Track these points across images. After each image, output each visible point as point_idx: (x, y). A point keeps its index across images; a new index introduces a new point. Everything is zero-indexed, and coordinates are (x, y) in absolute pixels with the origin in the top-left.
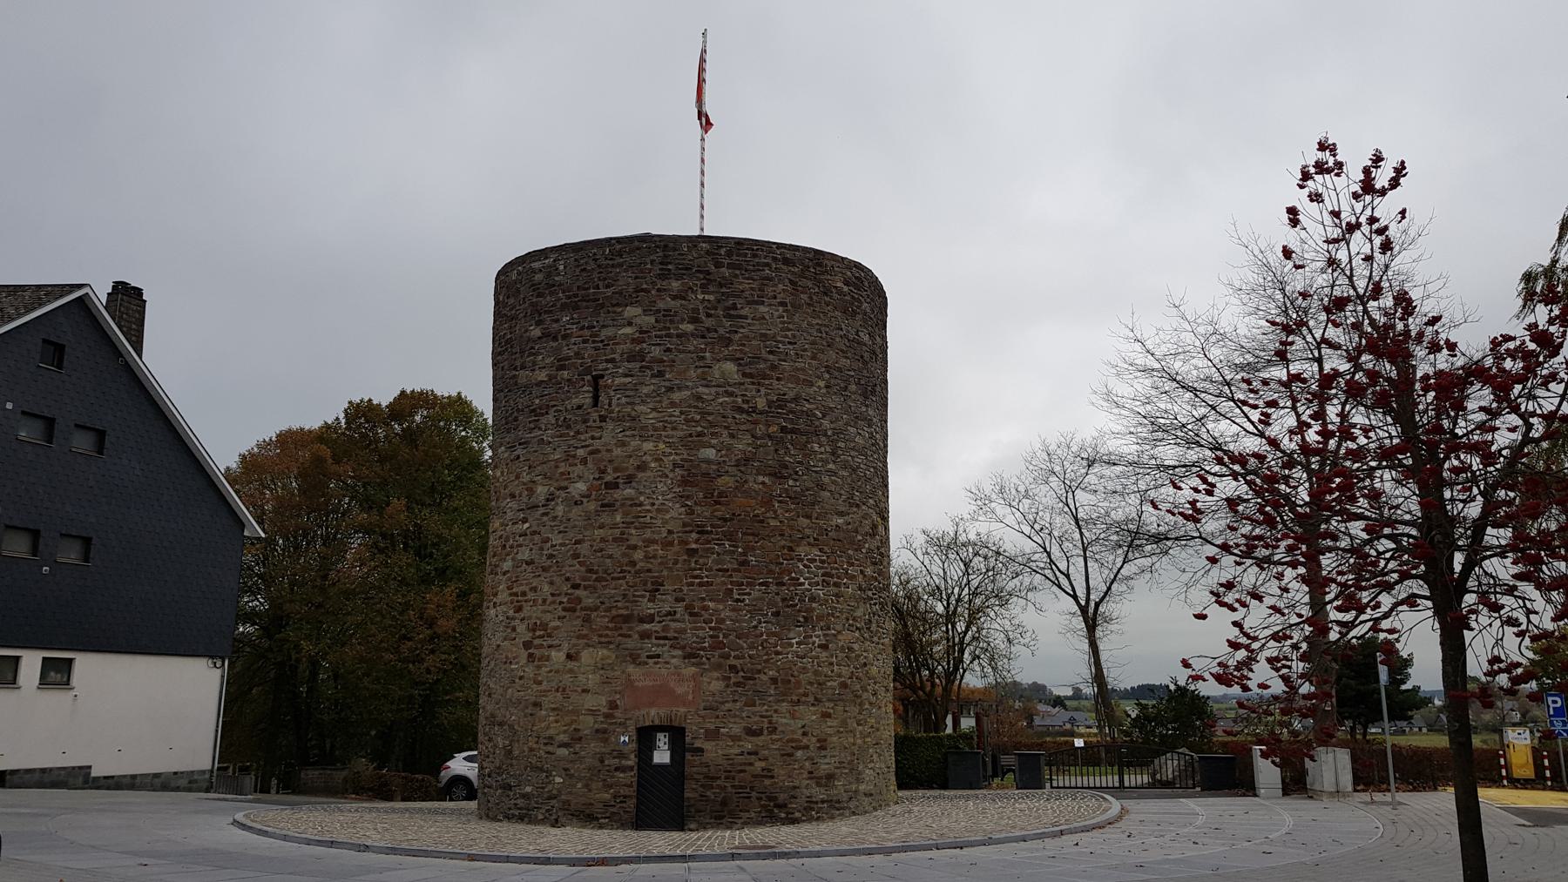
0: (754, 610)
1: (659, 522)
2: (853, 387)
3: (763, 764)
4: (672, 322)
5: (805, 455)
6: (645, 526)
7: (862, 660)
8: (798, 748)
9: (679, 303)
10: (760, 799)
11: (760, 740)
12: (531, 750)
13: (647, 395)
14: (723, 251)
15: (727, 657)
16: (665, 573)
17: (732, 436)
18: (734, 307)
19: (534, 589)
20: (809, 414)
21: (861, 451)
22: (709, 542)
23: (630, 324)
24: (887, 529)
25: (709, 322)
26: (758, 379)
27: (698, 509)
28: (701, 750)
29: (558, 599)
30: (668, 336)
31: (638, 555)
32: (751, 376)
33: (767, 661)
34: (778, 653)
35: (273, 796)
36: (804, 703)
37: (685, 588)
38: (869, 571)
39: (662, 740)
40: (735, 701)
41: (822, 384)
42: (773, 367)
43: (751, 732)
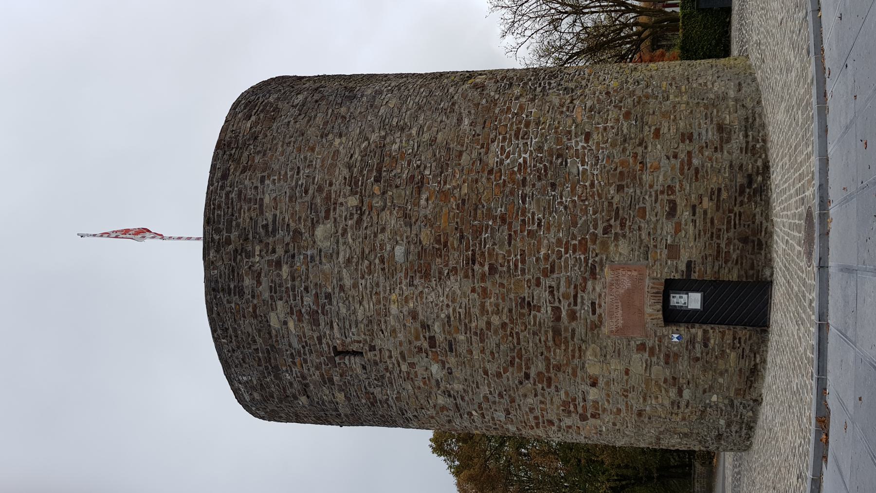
0: (549, 209)
1: (465, 301)
2: (343, 110)
3: (706, 200)
4: (281, 286)
5: (402, 159)
6: (468, 314)
7: (603, 97)
8: (690, 163)
9: (263, 279)
10: (742, 204)
11: (681, 203)
12: (684, 419)
13: (348, 309)
14: (216, 237)
15: (595, 237)
16: (512, 296)
17: (383, 230)
18: (265, 227)
19: (532, 410)
20: (364, 154)
21: (403, 100)
22: (483, 254)
23: (285, 323)
24: (481, 73)
25: (280, 251)
26: (330, 204)
27: (452, 263)
28: (689, 264)
29: (539, 391)
30: (293, 289)
31: (496, 320)
32: (328, 212)
33: (600, 196)
34: (592, 185)
36: (643, 157)
37: (527, 277)
38: (517, 91)
39: (678, 300)
40: (640, 228)
41: (337, 141)
42: (320, 189)
43: (672, 212)
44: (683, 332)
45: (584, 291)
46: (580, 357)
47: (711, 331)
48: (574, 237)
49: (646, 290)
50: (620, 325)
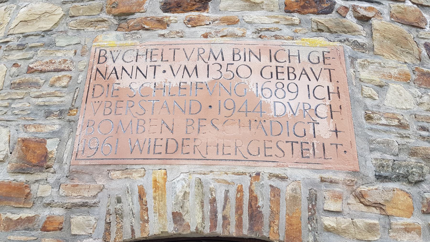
49: (266, 169)
50: (125, 81)
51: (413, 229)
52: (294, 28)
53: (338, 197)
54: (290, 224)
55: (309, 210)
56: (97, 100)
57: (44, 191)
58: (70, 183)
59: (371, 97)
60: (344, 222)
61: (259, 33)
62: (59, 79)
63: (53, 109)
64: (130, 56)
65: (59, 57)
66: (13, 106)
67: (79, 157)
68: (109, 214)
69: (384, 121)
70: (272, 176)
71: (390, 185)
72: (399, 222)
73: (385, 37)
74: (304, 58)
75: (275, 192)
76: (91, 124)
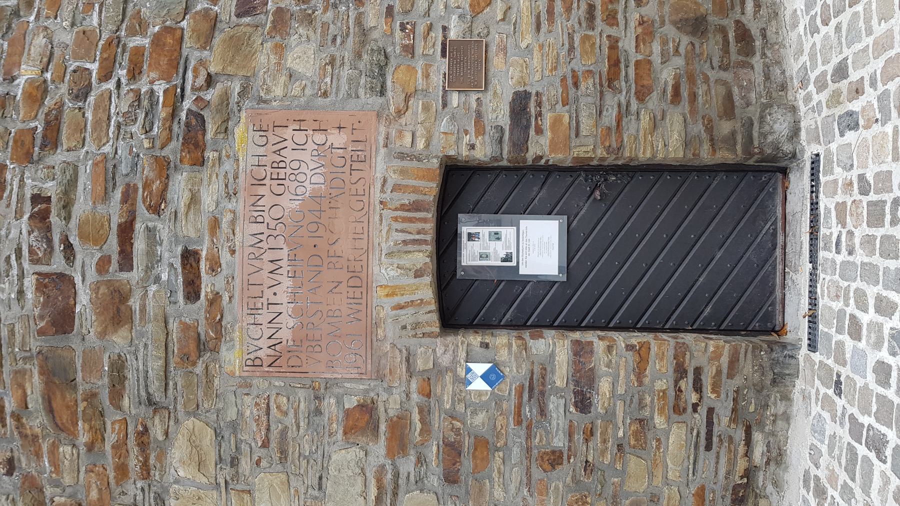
28: (520, 105)
35: (572, 357)
39: (483, 246)
44: (503, 355)
45: (156, 210)
46: (146, 471)
47: (600, 346)
48: (140, 27)
49: (376, 195)
50: (285, 334)
51: (427, 71)
52: (224, 158)
53: (400, 133)
54: (423, 178)
55: (411, 160)
56: (305, 362)
57: (395, 402)
58: (388, 377)
59: (304, 89)
60: (420, 131)
61: (231, 194)
62: (278, 407)
63: (313, 407)
64: (255, 332)
65: (251, 413)
66: (307, 454)
67: (364, 371)
68: (415, 336)
69: (328, 80)
70: (382, 191)
71: (389, 83)
72: (420, 82)
73: (231, 62)
74: (261, 151)
75: (396, 188)
76: (330, 364)
